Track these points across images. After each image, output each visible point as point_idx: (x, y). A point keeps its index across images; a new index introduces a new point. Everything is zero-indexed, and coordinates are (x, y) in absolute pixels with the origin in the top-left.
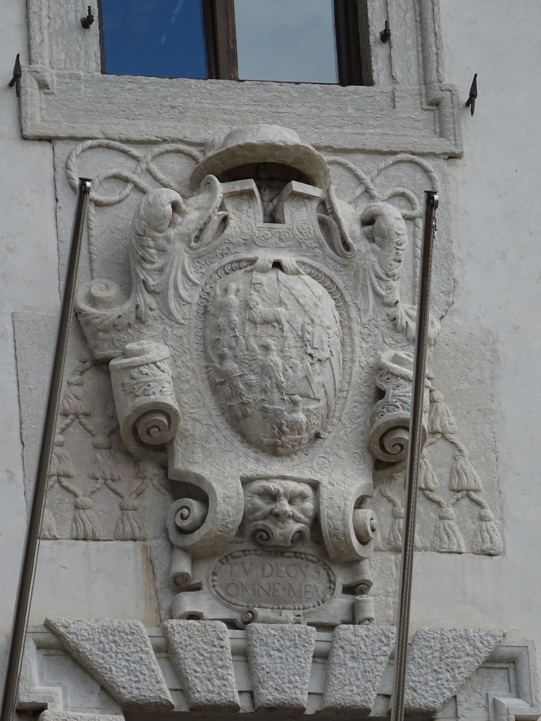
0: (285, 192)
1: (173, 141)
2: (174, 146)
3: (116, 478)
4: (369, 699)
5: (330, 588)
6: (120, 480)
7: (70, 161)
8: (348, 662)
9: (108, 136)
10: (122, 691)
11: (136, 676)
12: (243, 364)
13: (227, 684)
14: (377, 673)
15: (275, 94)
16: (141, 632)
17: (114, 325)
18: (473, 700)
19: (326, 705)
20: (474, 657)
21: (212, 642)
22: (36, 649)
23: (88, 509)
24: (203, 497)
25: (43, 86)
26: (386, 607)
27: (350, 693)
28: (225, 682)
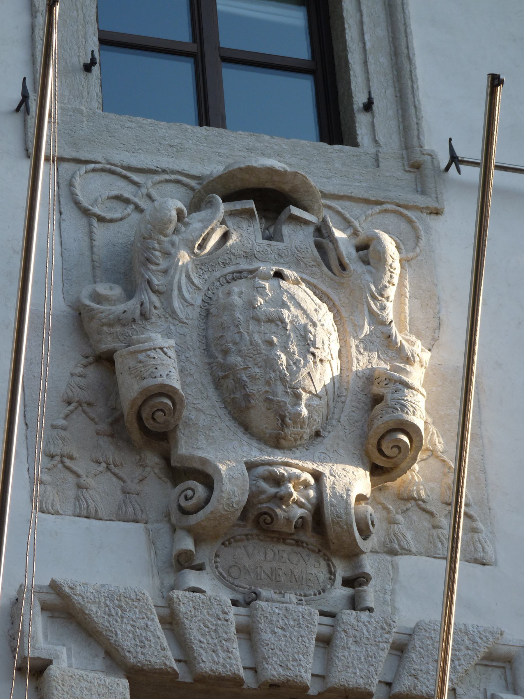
0: (283, 216)
1: (172, 172)
2: (173, 177)
3: (118, 463)
4: (372, 682)
5: (330, 579)
7: (74, 180)
8: (350, 645)
9: (110, 162)
10: (127, 654)
11: (141, 642)
12: (248, 358)
13: (232, 656)
15: (266, 144)
16: (147, 600)
17: (119, 320)
19: (329, 685)
20: (473, 650)
21: (218, 615)
22: (40, 609)
24: (208, 480)
26: (384, 603)
27: (353, 675)
28: (230, 655)
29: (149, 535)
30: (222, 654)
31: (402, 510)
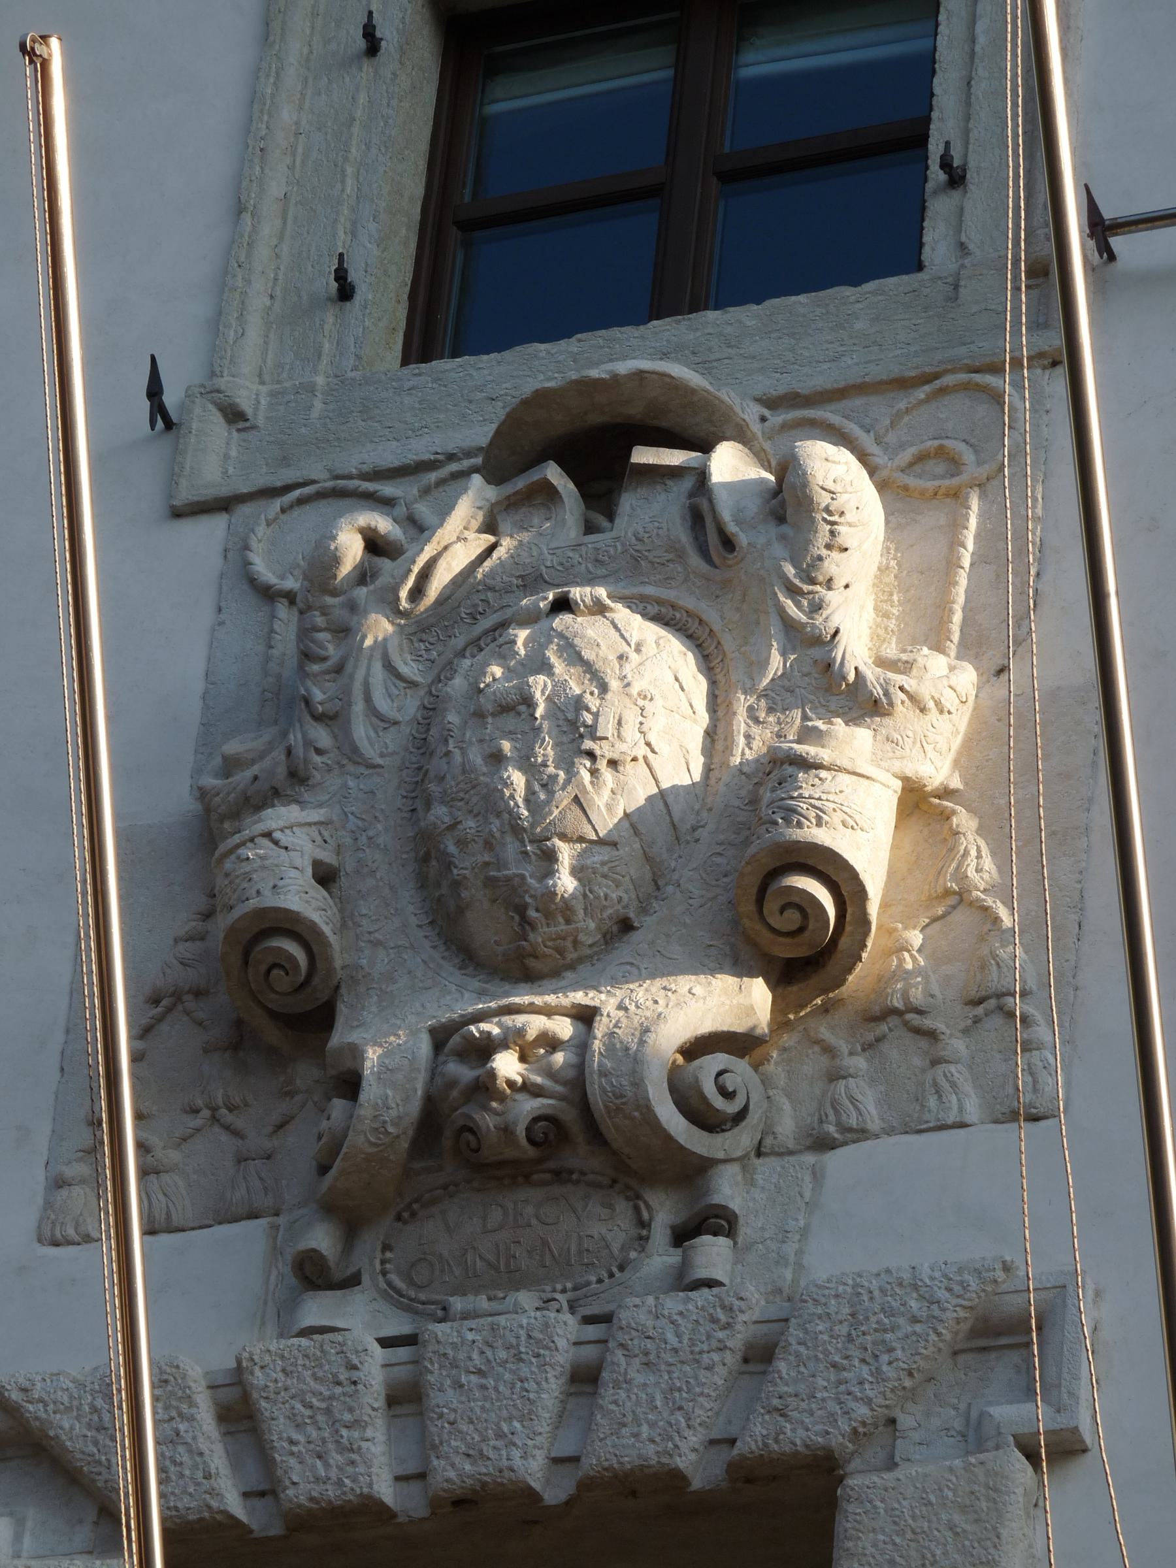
4: (676, 1446)
6: (246, 1105)
14: (698, 1390)
17: (247, 799)
18: (936, 1422)
23: (167, 1172)
25: (234, 416)
29: (275, 1239)
30: (336, 1458)
31: (863, 1045)
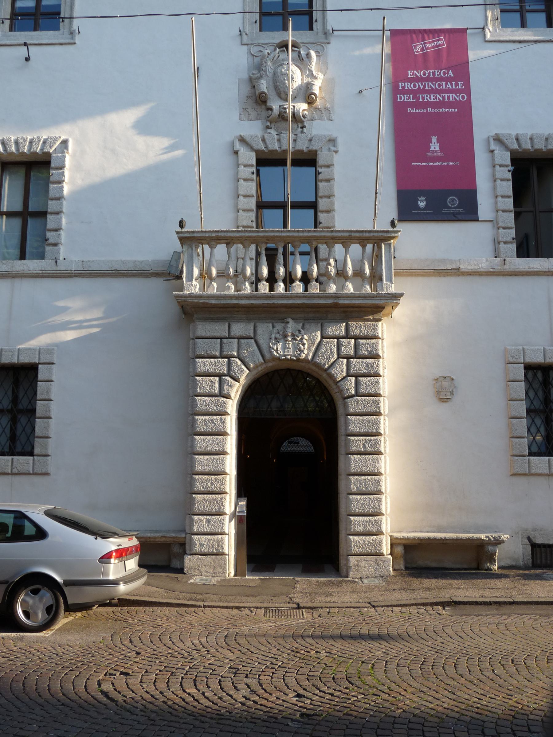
25: (246, 34)
